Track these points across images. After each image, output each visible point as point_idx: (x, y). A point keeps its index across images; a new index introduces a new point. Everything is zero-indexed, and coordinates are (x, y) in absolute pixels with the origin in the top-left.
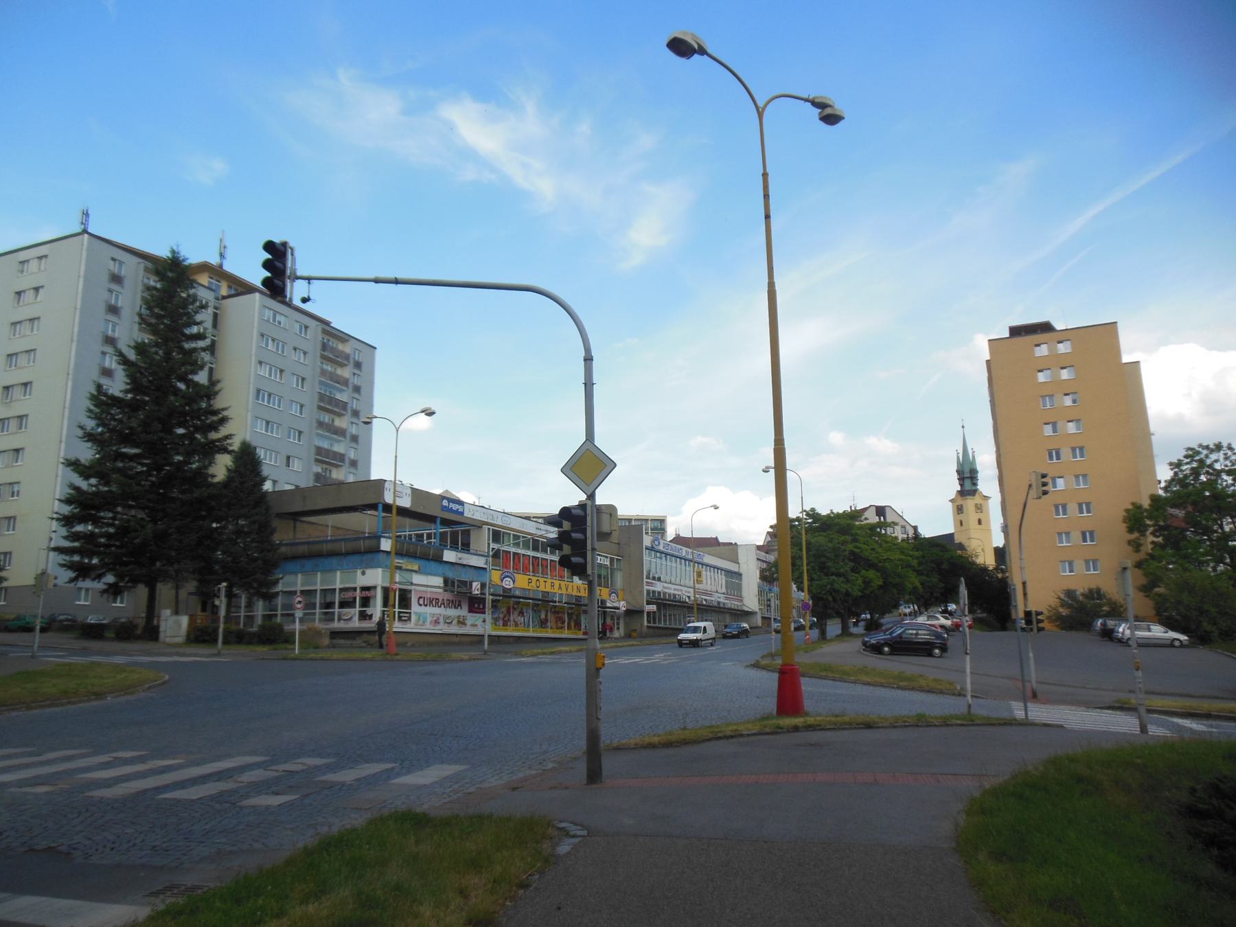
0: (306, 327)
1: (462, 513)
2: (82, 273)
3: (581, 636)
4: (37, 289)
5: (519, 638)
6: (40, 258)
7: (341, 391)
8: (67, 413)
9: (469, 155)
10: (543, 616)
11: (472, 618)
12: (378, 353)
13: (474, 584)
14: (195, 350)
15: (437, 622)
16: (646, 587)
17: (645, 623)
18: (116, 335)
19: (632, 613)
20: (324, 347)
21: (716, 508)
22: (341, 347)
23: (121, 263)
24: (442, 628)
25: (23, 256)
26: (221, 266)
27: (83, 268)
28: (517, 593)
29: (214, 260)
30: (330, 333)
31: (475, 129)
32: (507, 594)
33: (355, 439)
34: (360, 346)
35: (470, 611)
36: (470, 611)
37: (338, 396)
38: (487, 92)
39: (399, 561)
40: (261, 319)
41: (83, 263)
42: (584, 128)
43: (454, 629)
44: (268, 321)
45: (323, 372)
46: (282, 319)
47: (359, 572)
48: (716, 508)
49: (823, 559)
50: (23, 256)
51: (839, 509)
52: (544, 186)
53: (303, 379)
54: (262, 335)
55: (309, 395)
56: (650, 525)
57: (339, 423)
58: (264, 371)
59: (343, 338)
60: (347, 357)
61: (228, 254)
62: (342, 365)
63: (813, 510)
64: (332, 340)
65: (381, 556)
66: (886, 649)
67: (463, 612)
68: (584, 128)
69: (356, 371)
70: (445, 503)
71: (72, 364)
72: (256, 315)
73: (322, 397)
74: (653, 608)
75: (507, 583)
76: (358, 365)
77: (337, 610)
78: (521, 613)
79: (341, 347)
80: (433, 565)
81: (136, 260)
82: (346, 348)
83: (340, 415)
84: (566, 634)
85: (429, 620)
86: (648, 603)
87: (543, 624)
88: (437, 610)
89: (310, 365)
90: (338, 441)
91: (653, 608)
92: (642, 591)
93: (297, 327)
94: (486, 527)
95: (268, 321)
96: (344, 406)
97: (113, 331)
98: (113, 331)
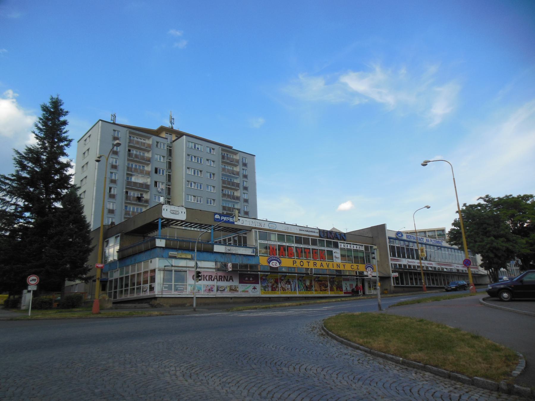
0: (213, 149)
1: (233, 223)
2: (99, 138)
3: (343, 295)
4: (88, 150)
5: (288, 298)
6: (89, 136)
7: (237, 178)
8: (94, 202)
9: (355, 94)
10: (308, 283)
11: (242, 287)
12: (256, 159)
13: (229, 264)
14: (62, 146)
15: (211, 290)
16: (390, 262)
17: (393, 285)
18: (117, 164)
19: (384, 279)
20: (223, 157)
21: (428, 207)
22: (235, 157)
23: (118, 131)
24: (214, 294)
25: (85, 138)
26: (172, 128)
27: (99, 136)
28: (284, 270)
29: (168, 125)
30: (227, 150)
31: (356, 83)
32: (274, 270)
33: (246, 201)
34: (245, 155)
35: (240, 282)
36: (240, 282)
37: (235, 181)
38: (359, 67)
39: (172, 253)
40: (187, 148)
41: (99, 134)
42: (403, 71)
43: (227, 294)
44: (192, 148)
45: (224, 169)
46: (199, 147)
47: (150, 261)
48: (428, 207)
49: (484, 226)
50: (85, 138)
51: (515, 195)
52: (389, 99)
53: (214, 174)
54: (189, 155)
55: (217, 181)
56: (436, 233)
57: (237, 194)
58: (191, 172)
59: (236, 152)
60: (238, 161)
61: (176, 122)
62: (236, 166)
63: (487, 196)
64: (229, 154)
65: (158, 250)
66: (505, 295)
67: (235, 283)
68: (403, 71)
69: (244, 168)
70: (217, 216)
71: (96, 179)
72: (185, 146)
73: (224, 182)
74: (396, 274)
75: (274, 264)
76: (245, 165)
77: (142, 286)
78: (288, 282)
79: (235, 157)
80: (205, 255)
81: (126, 129)
82: (236, 157)
83: (237, 190)
84: (329, 294)
85: (203, 289)
86: (393, 272)
87: (308, 288)
88: (210, 283)
89: (216, 167)
90: (237, 203)
91: (396, 274)
92: (388, 265)
93: (208, 150)
94: (253, 230)
95: (192, 148)
96: (238, 185)
97: (116, 162)
98: (116, 162)
